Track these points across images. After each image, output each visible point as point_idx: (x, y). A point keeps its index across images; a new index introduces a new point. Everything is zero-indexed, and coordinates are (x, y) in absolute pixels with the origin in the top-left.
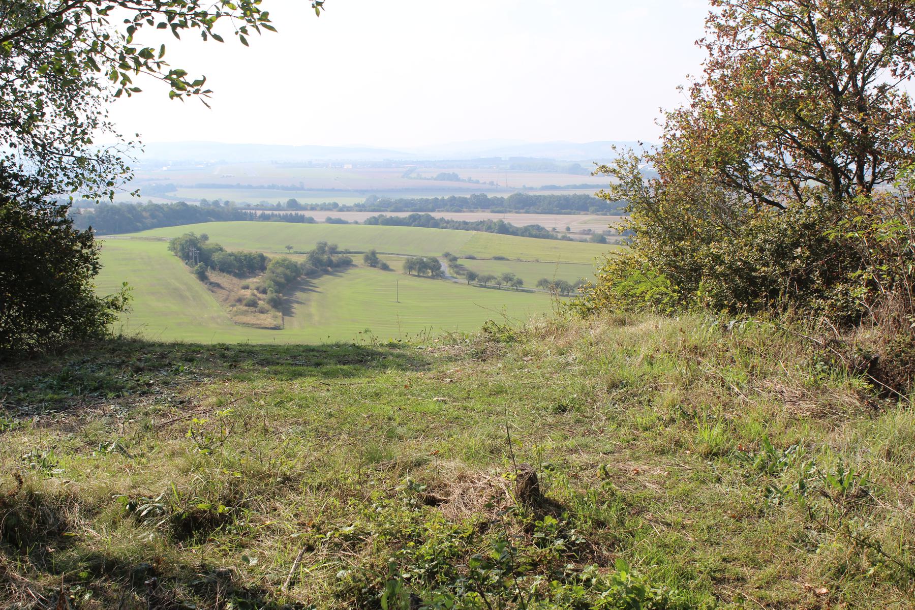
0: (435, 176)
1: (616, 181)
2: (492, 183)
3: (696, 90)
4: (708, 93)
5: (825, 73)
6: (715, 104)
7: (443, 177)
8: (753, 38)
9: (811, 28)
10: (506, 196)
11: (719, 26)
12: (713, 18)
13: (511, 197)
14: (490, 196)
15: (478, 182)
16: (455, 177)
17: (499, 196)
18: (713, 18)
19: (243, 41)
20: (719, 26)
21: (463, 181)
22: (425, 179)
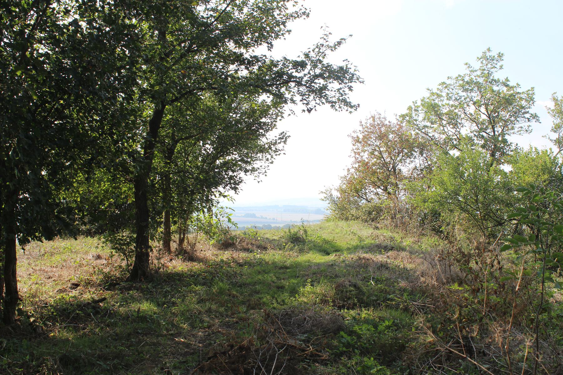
0: (243, 215)
1: (326, 196)
2: (274, 219)
3: (348, 170)
4: (352, 171)
5: (385, 164)
6: (354, 174)
7: (247, 215)
8: (365, 156)
9: (380, 153)
10: (281, 226)
11: (355, 152)
12: (353, 150)
13: (284, 226)
14: (273, 225)
15: (266, 218)
16: (254, 216)
17: (278, 225)
18: (353, 150)
19: (466, 64)
20: (355, 152)
21: (258, 217)
22: (238, 216)
